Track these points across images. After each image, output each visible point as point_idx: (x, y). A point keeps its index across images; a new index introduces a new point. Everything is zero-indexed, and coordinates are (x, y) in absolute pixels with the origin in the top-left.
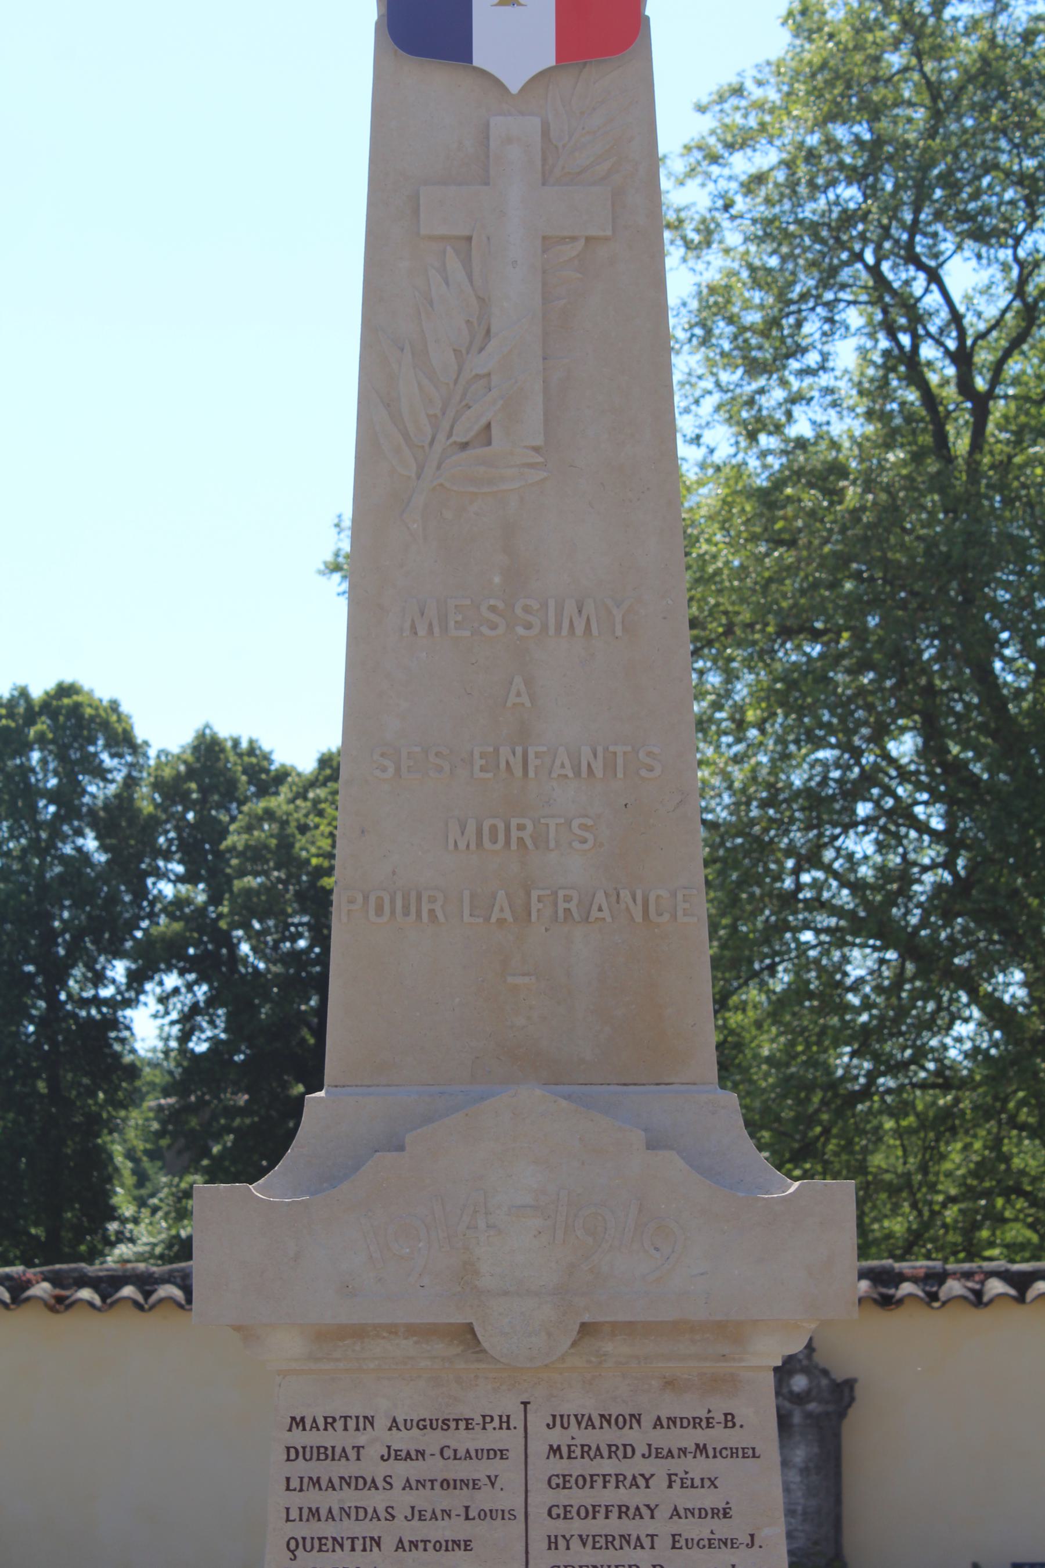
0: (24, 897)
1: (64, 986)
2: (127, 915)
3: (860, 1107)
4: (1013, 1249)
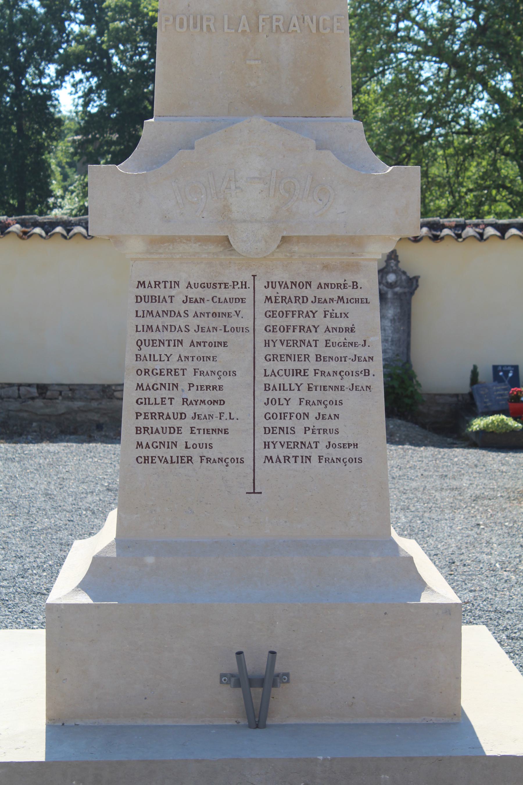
0: (2, 31)
1: (24, 77)
2: (55, 41)
3: (426, 144)
4: (499, 215)
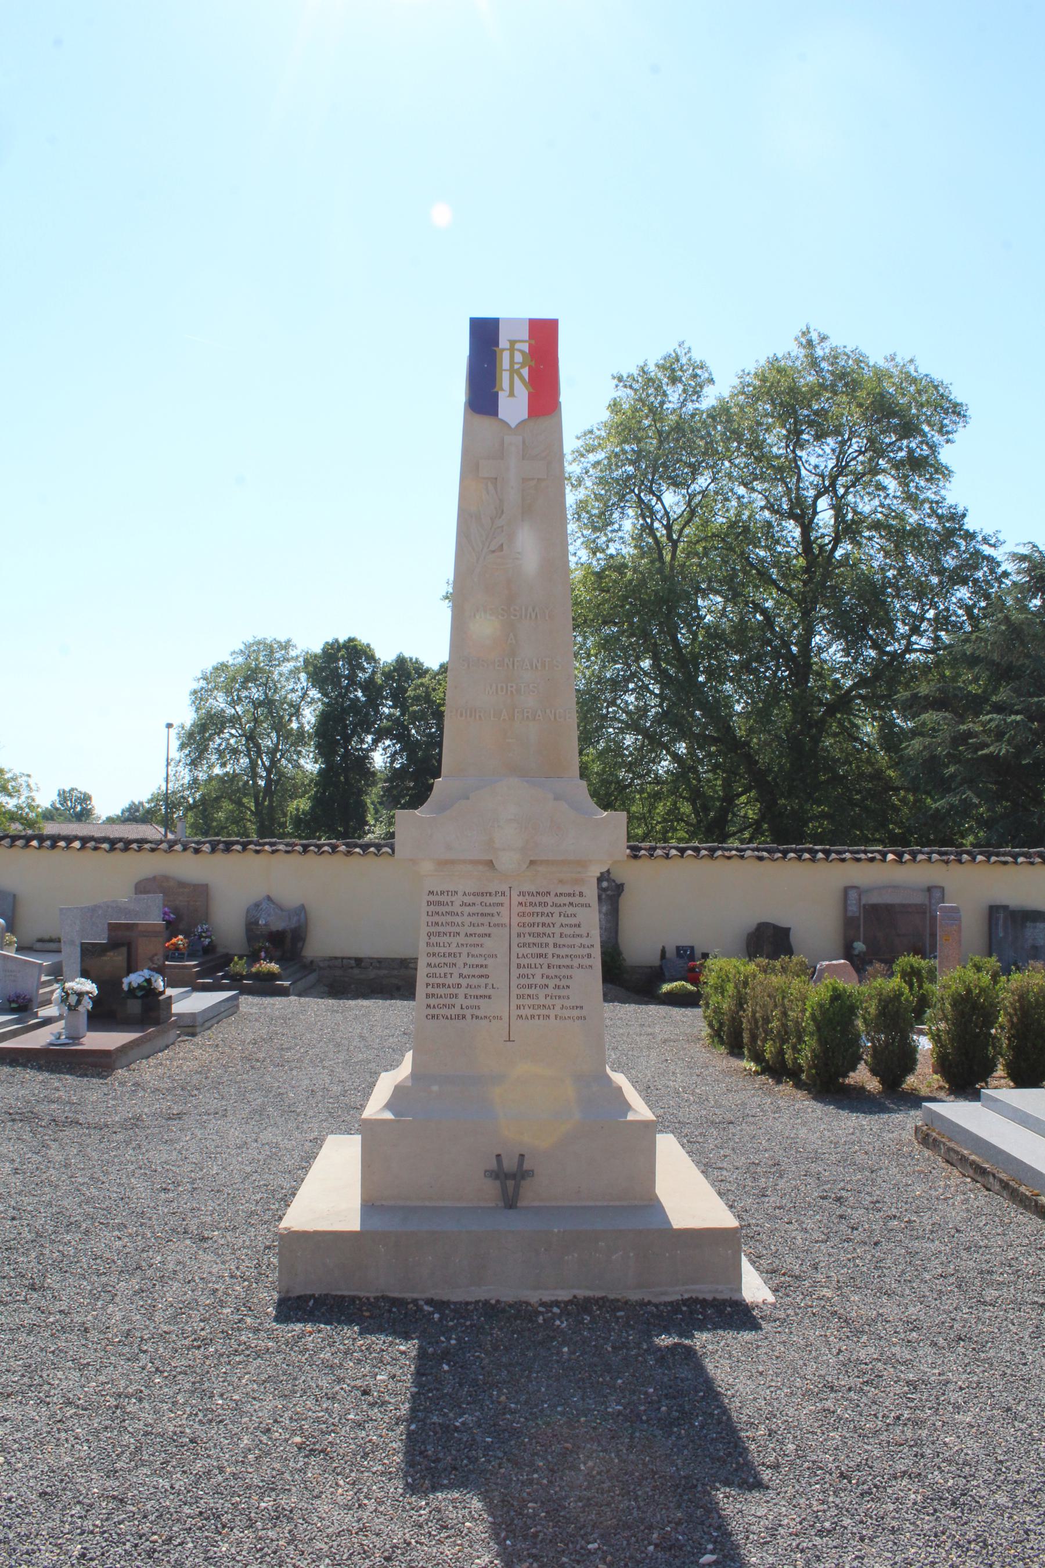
4: (680, 840)
